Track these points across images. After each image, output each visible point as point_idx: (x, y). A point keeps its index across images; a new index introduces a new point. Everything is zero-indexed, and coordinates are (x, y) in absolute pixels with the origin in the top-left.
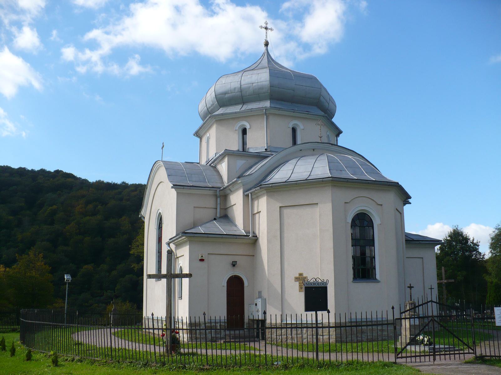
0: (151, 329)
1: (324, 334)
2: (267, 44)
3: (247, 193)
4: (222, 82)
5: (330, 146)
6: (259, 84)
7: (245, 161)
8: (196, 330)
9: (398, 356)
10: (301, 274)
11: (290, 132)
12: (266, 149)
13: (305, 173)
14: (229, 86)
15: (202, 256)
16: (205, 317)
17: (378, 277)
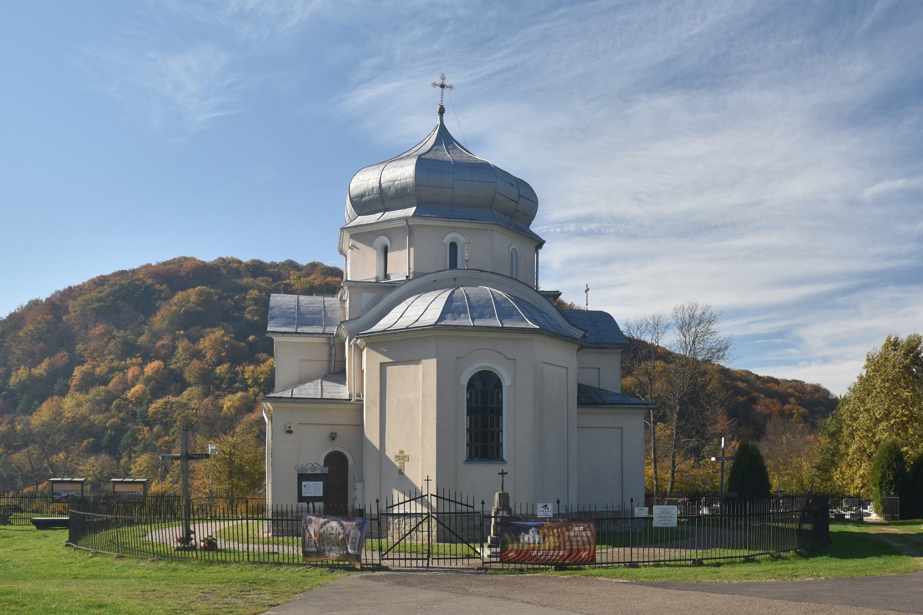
1: (424, 530)
2: (442, 111)
5: (478, 273)
6: (402, 181)
7: (375, 295)
8: (282, 520)
9: (384, 557)
10: (401, 452)
12: (407, 277)
15: (290, 427)
17: (505, 457)
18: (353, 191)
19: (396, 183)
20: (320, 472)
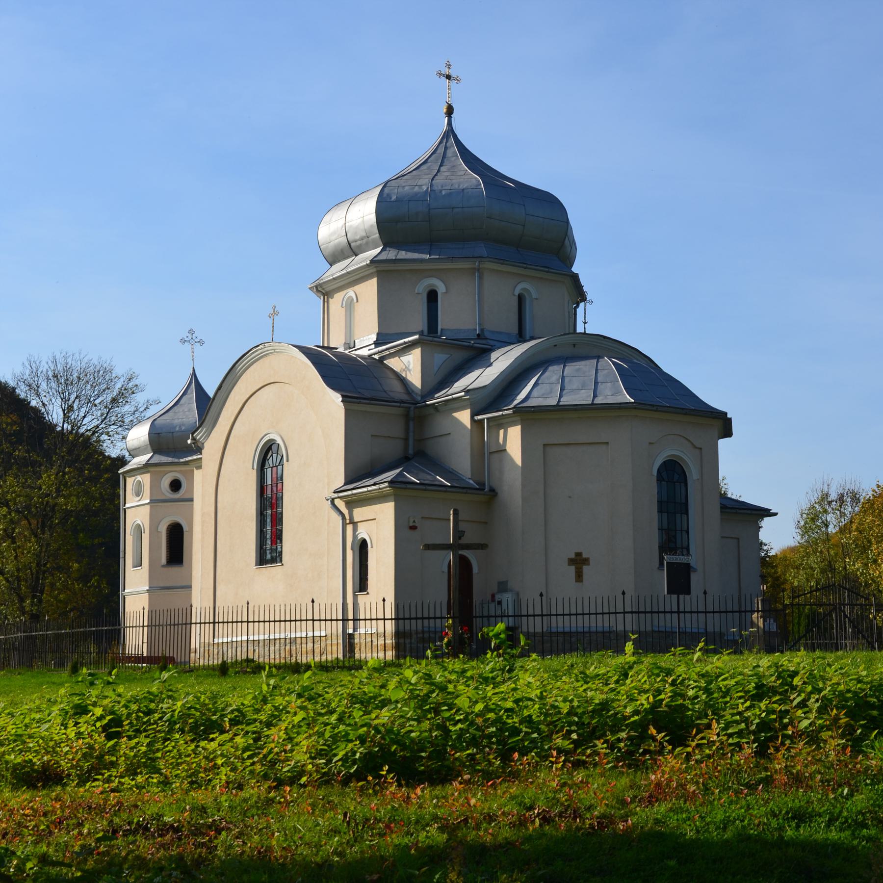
3: (480, 417)
4: (391, 198)
10: (579, 554)
15: (414, 521)
19: (456, 210)
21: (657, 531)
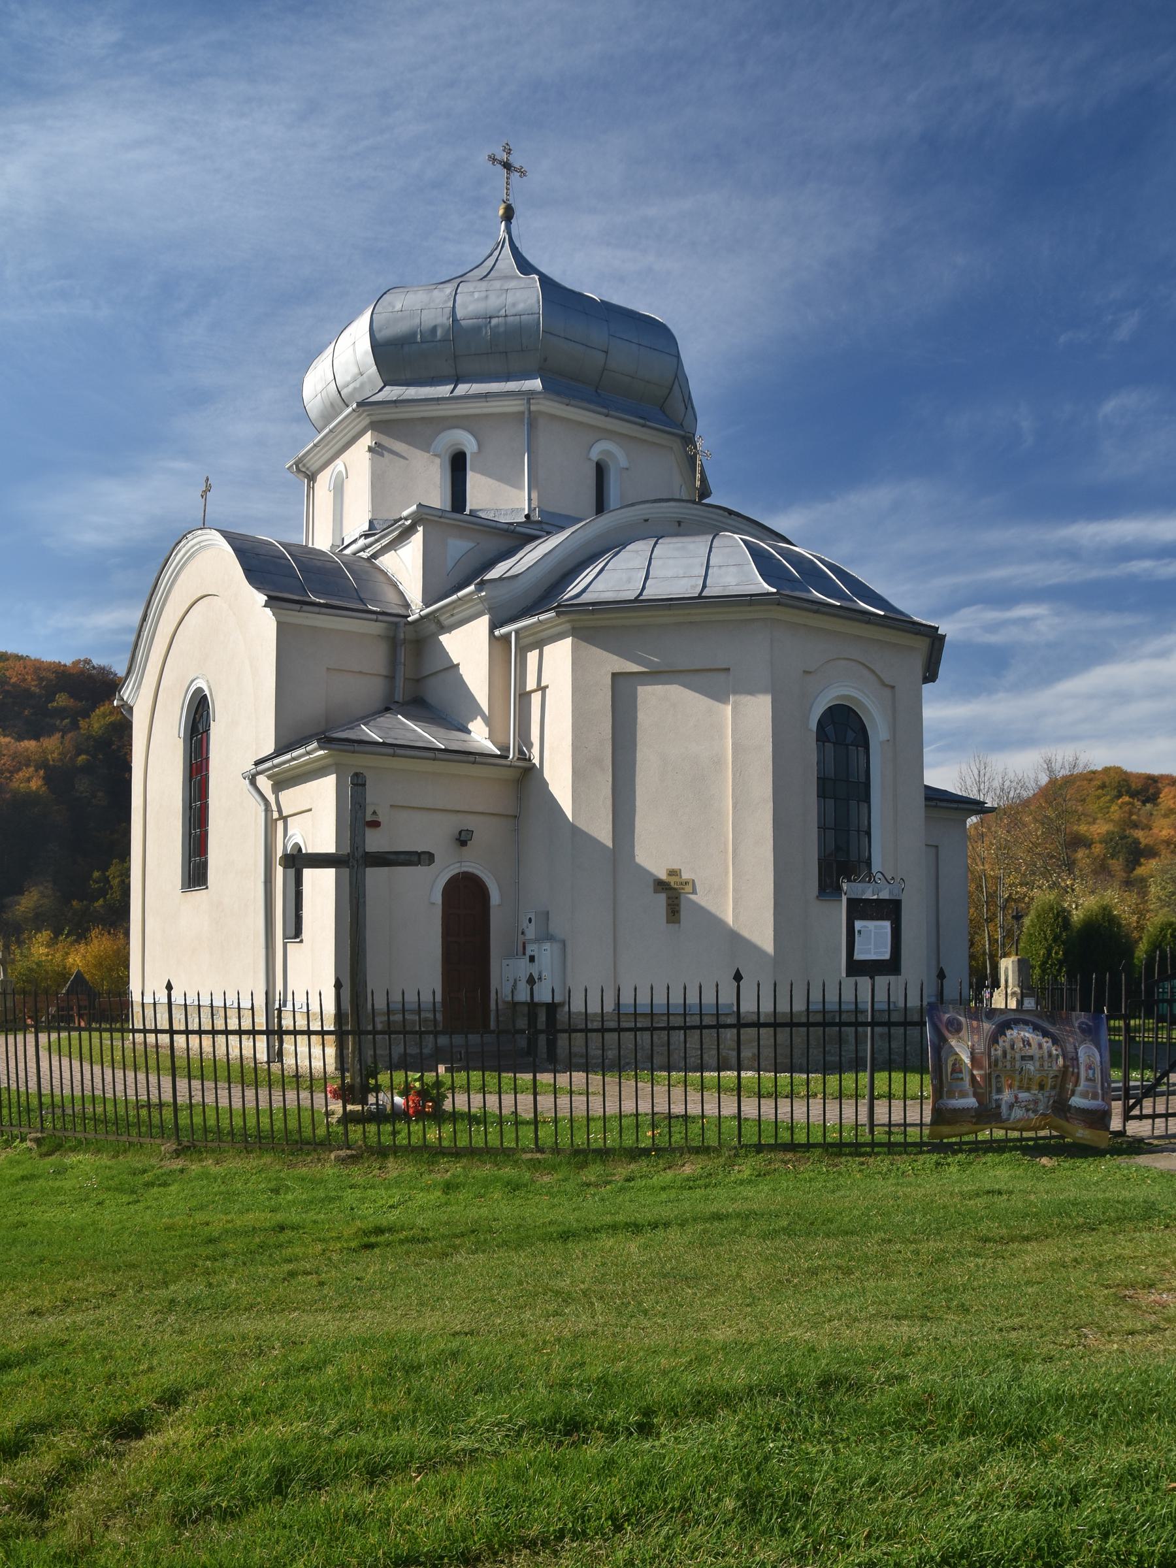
0: (163, 1032)
3: (504, 630)
4: (394, 307)
5: (724, 517)
6: (510, 319)
11: (592, 473)
13: (693, 582)
14: (417, 321)
15: (374, 813)
16: (532, 990)
18: (380, 331)
19: (494, 321)
20: (887, 897)
21: (816, 830)
